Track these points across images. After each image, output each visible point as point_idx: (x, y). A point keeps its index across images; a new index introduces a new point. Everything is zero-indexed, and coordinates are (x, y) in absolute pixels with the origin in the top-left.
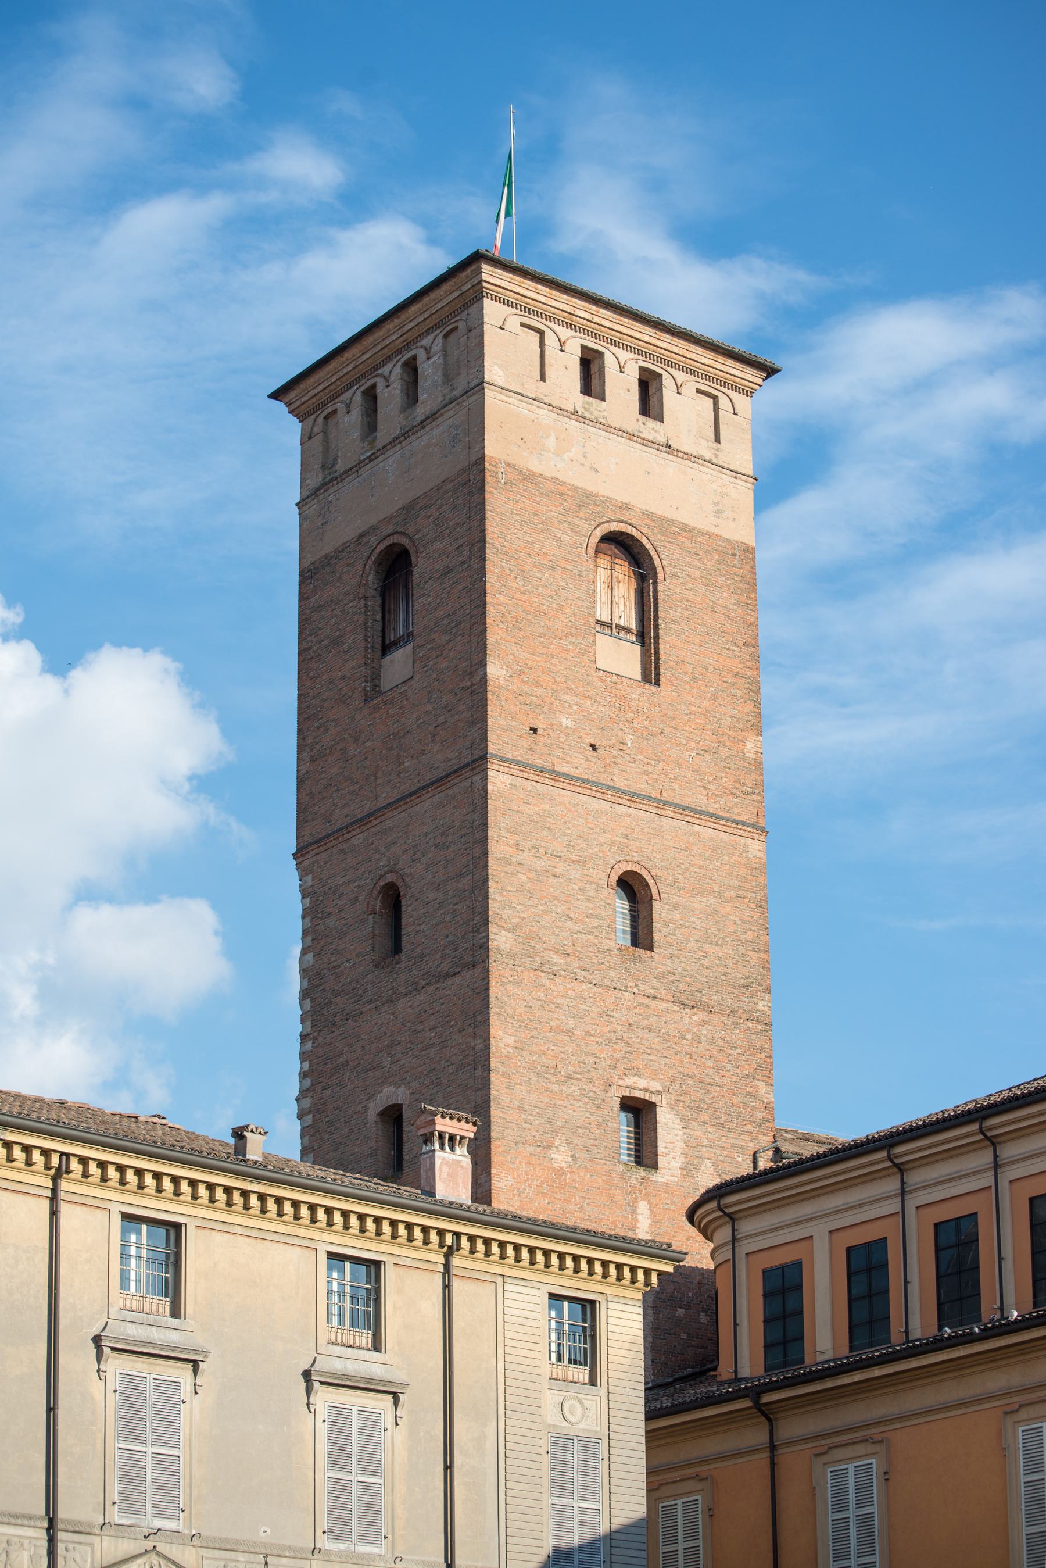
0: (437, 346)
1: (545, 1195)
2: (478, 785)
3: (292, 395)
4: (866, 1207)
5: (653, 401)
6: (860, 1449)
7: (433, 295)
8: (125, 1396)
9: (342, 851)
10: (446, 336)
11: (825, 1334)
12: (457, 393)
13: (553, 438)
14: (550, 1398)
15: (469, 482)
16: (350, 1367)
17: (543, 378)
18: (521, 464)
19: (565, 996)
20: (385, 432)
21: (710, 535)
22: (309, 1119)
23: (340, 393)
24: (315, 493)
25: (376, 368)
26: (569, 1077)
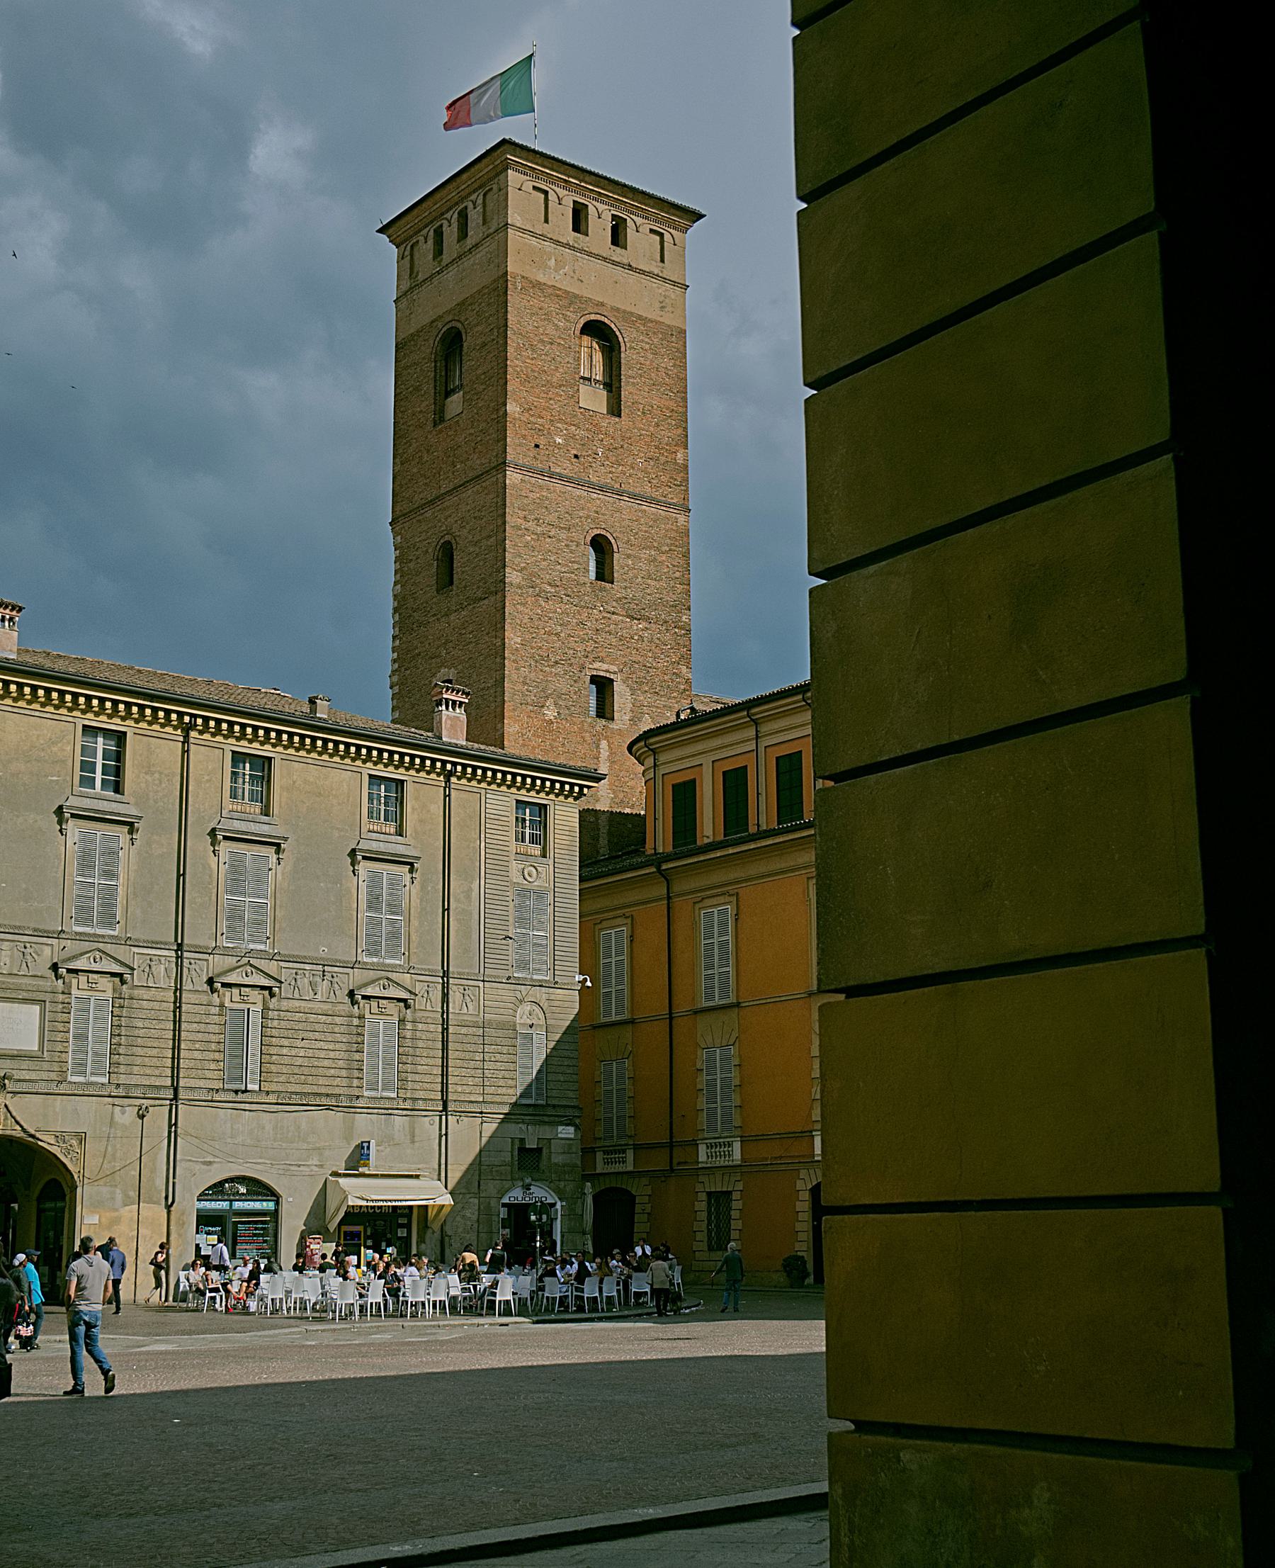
0: (480, 201)
1: (539, 737)
2: (501, 480)
3: (391, 231)
4: (735, 746)
5: (621, 236)
6: (722, 899)
7: (477, 167)
8: (231, 866)
9: (419, 521)
10: (485, 195)
11: (709, 824)
12: (491, 231)
13: (553, 260)
14: (515, 867)
15: (499, 288)
16: (382, 847)
17: (546, 221)
18: (532, 277)
19: (555, 612)
20: (448, 254)
21: (657, 322)
22: (396, 689)
23: (420, 231)
24: (405, 294)
25: (443, 214)
26: (556, 663)
